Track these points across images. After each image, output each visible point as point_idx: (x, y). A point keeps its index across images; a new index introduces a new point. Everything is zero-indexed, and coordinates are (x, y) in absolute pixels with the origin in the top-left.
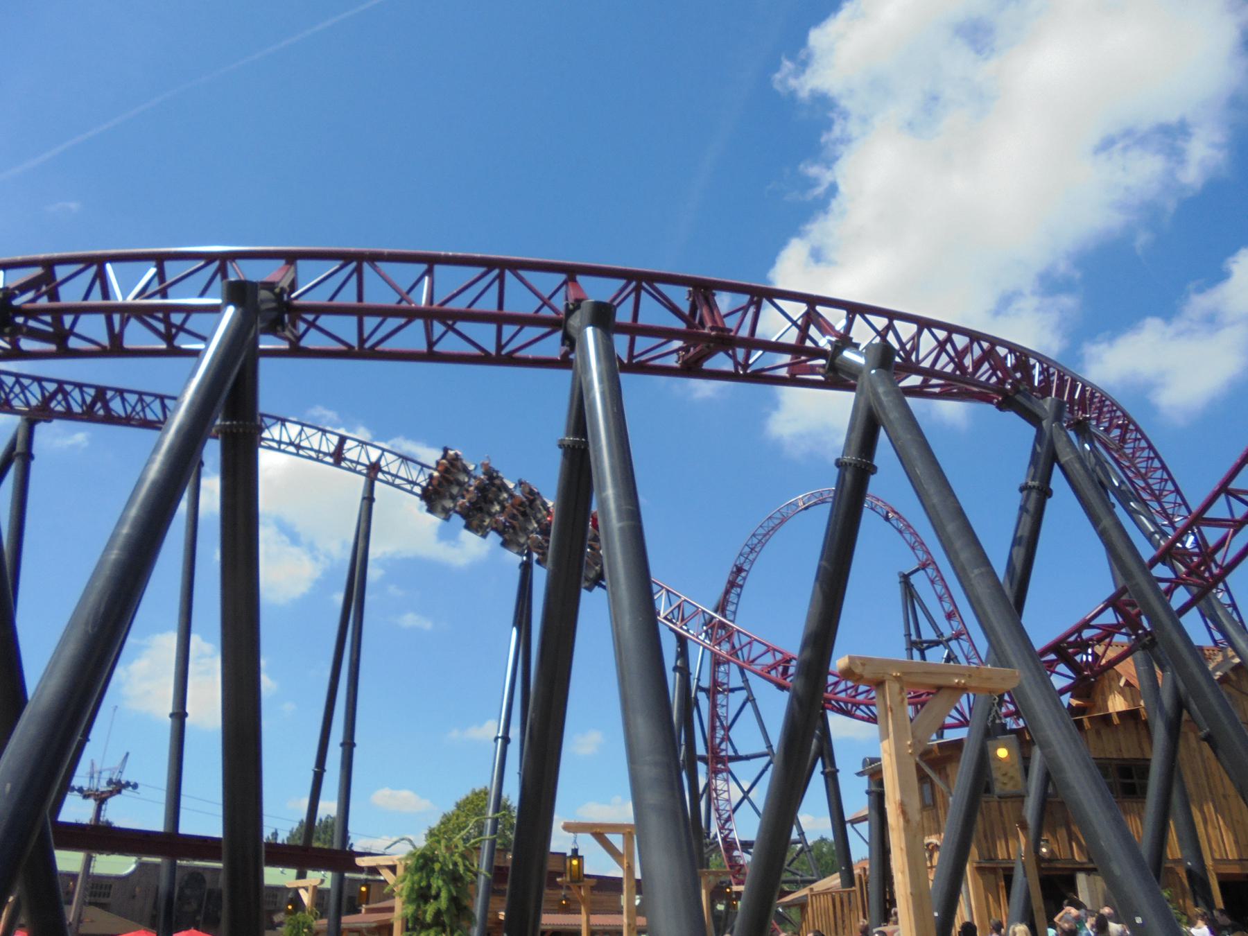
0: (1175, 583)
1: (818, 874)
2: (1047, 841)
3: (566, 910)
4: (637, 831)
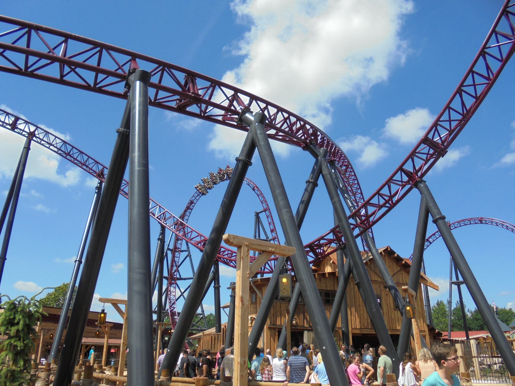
0: (356, 226)
1: (207, 328)
2: (296, 319)
3: (98, 336)
4: (129, 303)
